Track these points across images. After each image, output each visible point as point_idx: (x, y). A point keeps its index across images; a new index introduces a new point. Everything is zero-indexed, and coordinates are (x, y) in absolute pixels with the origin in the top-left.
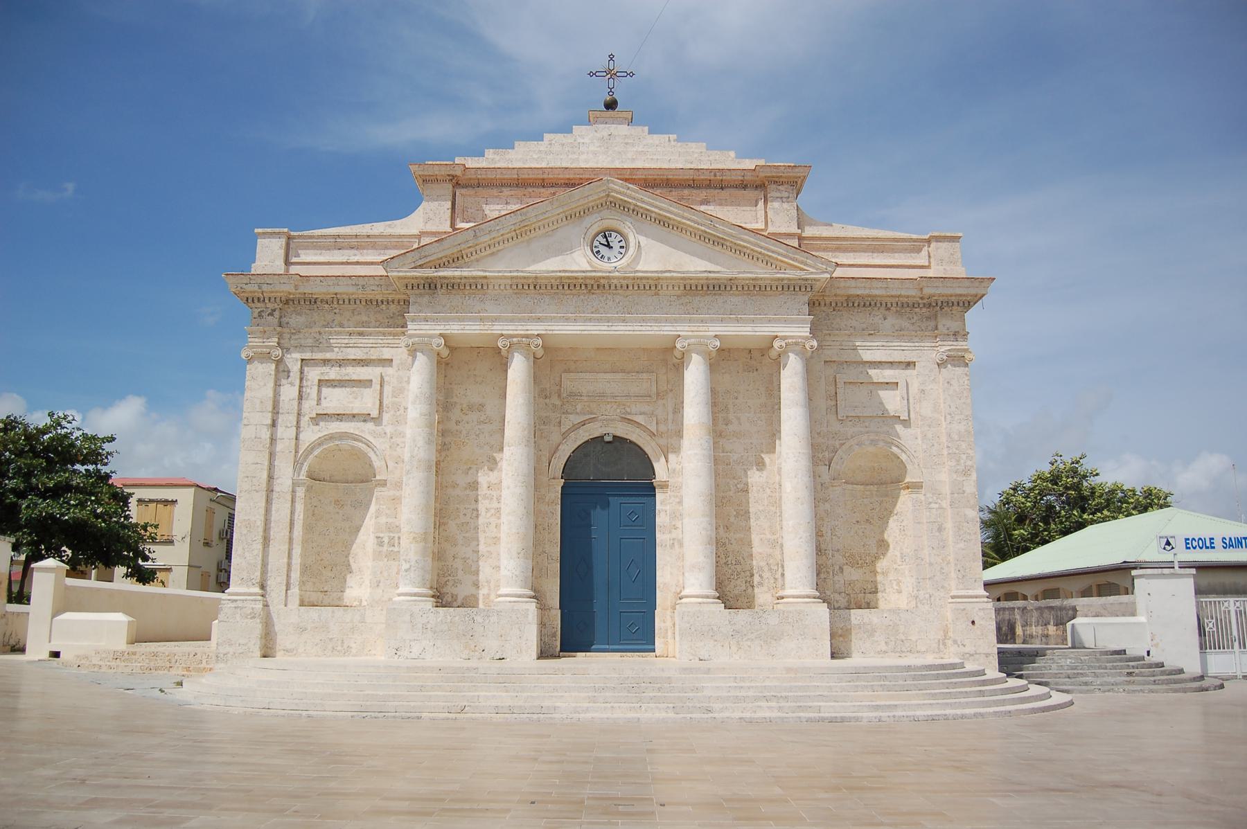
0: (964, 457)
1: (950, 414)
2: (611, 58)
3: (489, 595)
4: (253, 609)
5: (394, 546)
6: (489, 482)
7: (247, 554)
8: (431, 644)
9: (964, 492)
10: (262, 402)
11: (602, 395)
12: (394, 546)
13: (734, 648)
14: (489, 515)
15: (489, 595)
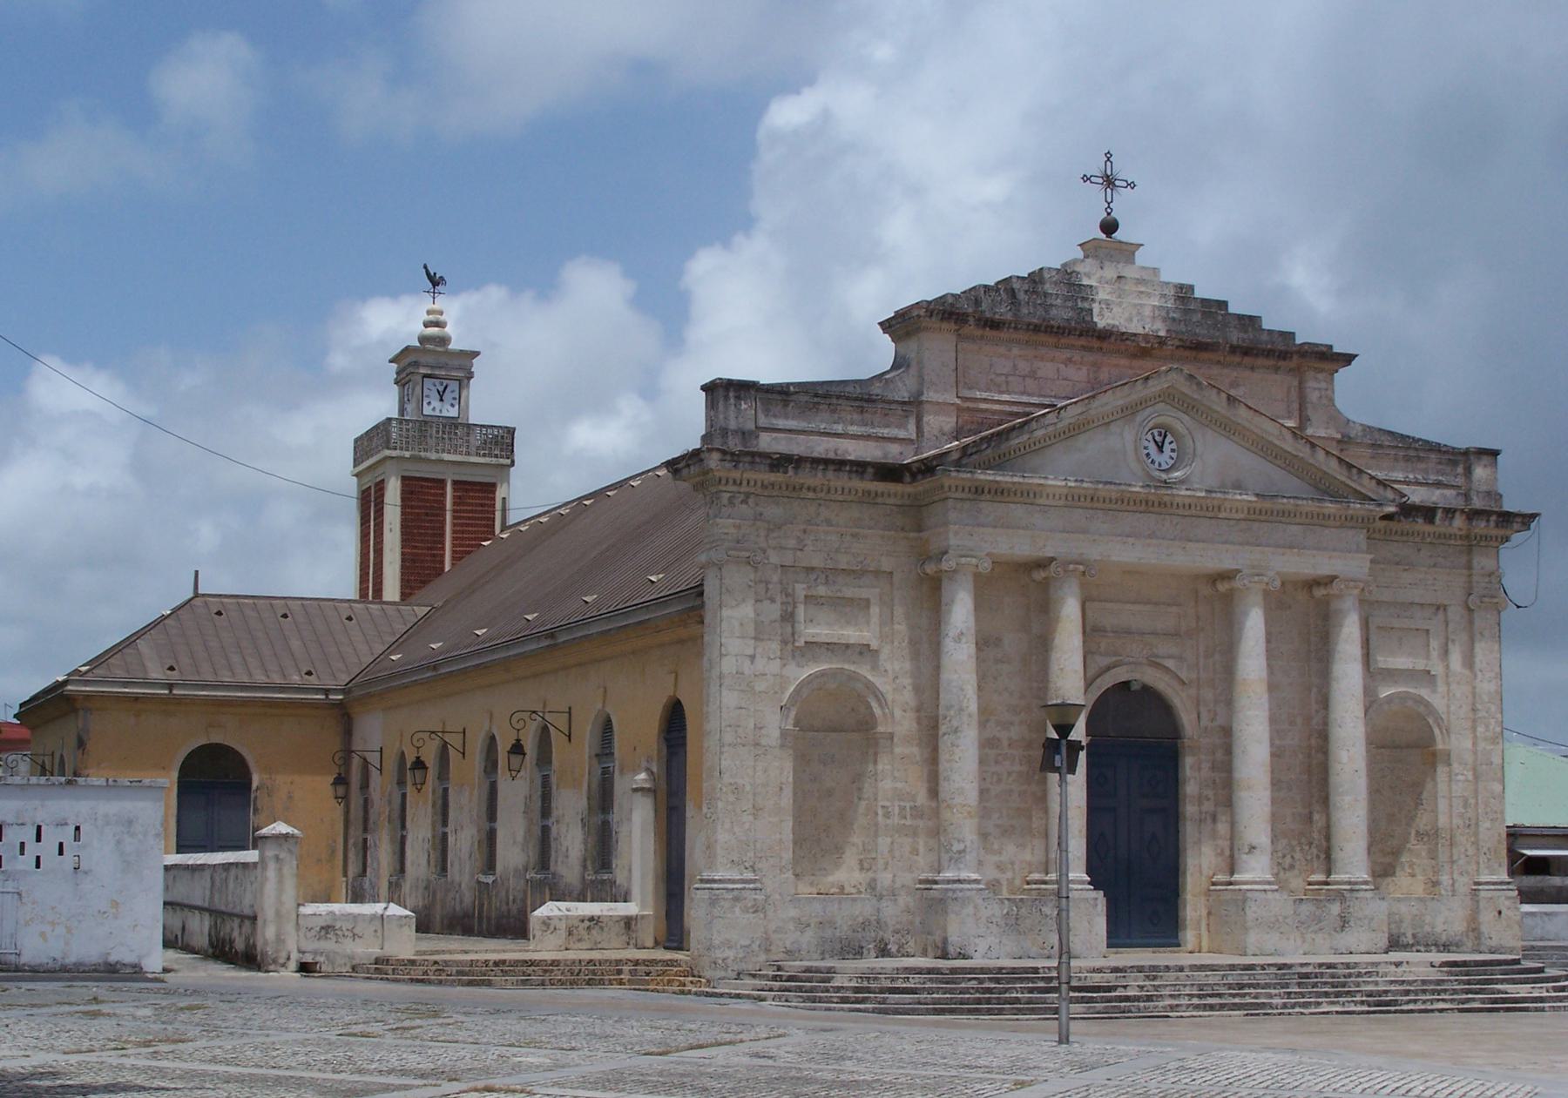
0: (1493, 721)
1: (1481, 671)
2: (1088, 179)
3: (1013, 879)
4: (755, 900)
5: (905, 818)
6: (1010, 739)
7: (736, 829)
8: (997, 941)
9: (1492, 763)
10: (741, 624)
11: (1128, 632)
12: (905, 818)
13: (1299, 941)
14: (1011, 779)
15: (1013, 879)
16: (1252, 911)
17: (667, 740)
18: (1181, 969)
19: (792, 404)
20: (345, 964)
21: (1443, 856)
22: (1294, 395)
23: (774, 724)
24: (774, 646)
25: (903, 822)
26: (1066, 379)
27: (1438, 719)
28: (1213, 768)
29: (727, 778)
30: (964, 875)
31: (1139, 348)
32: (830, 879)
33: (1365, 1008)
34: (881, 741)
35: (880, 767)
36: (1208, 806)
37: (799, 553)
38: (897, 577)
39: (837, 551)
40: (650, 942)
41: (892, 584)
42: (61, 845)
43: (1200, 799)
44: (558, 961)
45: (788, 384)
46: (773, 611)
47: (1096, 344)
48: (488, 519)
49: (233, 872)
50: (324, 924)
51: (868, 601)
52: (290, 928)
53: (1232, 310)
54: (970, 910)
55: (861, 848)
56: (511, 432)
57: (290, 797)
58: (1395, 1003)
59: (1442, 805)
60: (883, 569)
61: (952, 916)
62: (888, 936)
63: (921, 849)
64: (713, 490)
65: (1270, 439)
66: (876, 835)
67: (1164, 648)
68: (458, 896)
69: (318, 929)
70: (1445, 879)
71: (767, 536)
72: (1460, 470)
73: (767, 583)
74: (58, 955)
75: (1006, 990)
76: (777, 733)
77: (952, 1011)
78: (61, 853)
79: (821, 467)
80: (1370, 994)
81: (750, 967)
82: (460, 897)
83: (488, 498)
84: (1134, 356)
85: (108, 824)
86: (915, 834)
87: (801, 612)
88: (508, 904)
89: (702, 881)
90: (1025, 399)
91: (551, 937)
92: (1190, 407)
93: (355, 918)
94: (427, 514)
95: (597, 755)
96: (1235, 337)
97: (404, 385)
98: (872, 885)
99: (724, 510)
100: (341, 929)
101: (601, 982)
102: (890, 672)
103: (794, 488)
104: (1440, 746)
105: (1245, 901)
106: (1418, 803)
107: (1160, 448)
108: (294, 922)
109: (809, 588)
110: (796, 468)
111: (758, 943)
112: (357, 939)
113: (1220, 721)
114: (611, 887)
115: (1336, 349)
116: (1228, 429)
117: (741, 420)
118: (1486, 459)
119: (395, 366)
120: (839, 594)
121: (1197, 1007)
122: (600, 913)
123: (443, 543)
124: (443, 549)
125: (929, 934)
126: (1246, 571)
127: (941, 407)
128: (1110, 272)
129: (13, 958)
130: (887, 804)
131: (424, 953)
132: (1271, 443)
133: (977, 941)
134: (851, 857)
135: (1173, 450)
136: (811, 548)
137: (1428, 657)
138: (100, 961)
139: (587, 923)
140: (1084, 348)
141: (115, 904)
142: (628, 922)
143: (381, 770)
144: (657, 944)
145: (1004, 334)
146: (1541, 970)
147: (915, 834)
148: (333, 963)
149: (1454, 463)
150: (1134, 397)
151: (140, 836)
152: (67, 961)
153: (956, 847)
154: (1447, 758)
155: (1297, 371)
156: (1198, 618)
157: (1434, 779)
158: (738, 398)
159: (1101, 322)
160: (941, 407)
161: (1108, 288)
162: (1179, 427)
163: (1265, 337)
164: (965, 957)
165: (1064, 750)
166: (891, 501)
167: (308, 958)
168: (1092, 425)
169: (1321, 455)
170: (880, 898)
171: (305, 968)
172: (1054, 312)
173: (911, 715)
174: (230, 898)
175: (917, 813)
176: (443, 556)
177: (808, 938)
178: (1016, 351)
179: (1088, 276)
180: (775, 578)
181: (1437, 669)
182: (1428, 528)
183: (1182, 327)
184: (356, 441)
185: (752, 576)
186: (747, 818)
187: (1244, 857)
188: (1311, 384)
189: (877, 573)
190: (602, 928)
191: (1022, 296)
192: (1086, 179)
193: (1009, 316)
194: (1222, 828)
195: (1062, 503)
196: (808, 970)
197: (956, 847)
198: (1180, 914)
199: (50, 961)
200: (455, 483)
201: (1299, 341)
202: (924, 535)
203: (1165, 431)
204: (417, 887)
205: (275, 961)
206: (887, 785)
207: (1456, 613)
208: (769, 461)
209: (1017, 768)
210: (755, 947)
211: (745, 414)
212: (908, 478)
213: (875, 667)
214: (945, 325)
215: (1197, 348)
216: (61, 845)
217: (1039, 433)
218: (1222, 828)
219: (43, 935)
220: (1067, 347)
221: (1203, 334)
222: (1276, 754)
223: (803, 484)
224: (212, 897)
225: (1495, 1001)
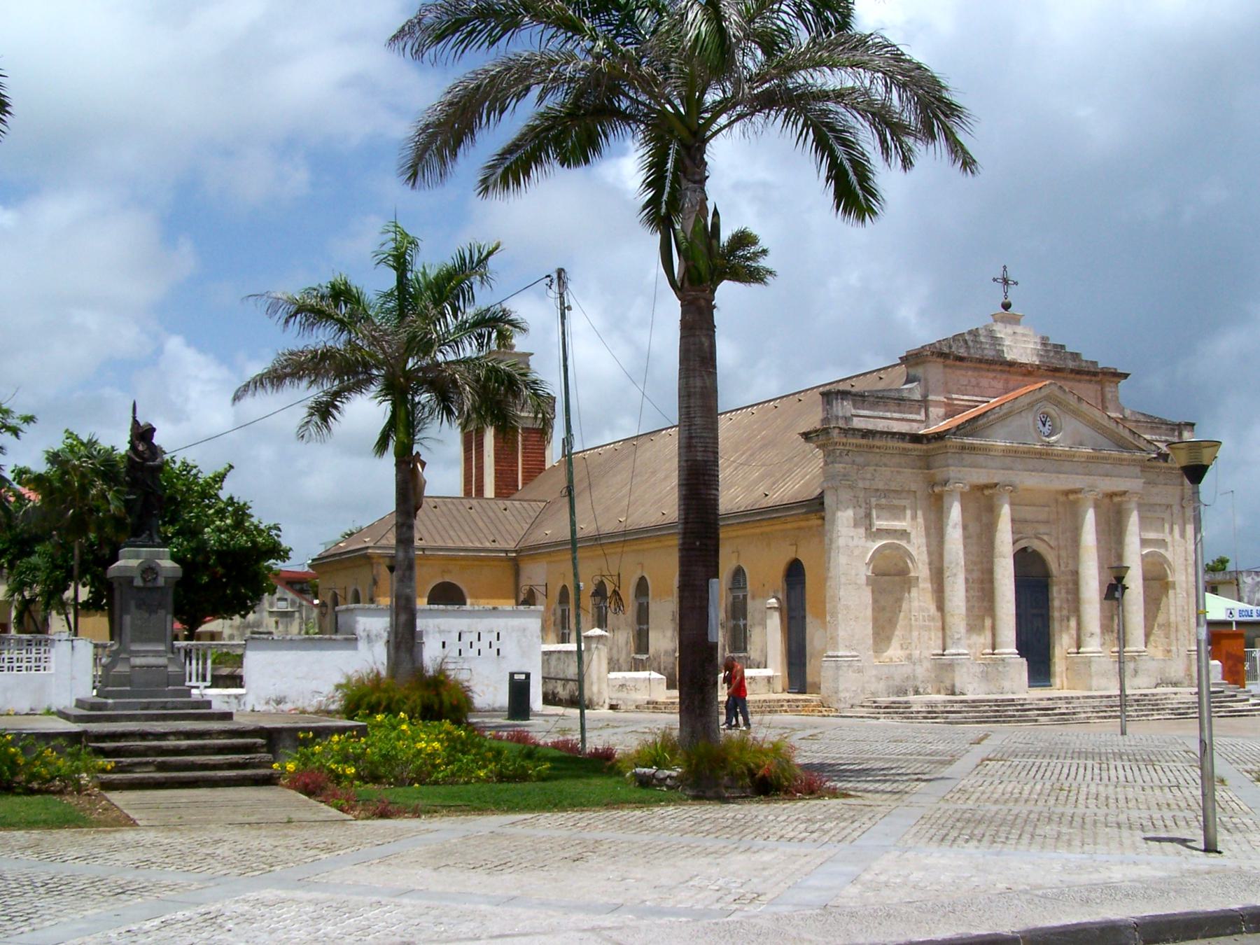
16: (1094, 668)
18: (1078, 698)
21: (1173, 636)
22: (1099, 393)
23: (864, 572)
24: (862, 531)
27: (1169, 565)
28: (1067, 592)
29: (843, 602)
30: (961, 651)
31: (1027, 371)
32: (885, 654)
33: (1173, 717)
35: (912, 595)
36: (1065, 612)
38: (918, 494)
40: (780, 690)
43: (1061, 609)
46: (862, 512)
47: (1007, 368)
49: (554, 657)
52: (604, 686)
53: (1067, 350)
54: (965, 669)
58: (1187, 714)
59: (1172, 610)
61: (957, 673)
62: (919, 684)
63: (933, 637)
64: (831, 448)
66: (911, 631)
67: (1042, 529)
70: (1174, 648)
72: (1176, 433)
75: (1006, 711)
76: (864, 578)
77: (985, 722)
80: (1172, 709)
81: (857, 702)
84: (1025, 375)
86: (930, 630)
87: (874, 513)
89: (827, 657)
90: (975, 398)
92: (1058, 403)
93: (636, 680)
96: (1071, 364)
98: (909, 657)
101: (776, 711)
104: (1170, 579)
105: (1090, 662)
106: (1158, 609)
107: (1044, 425)
110: (873, 437)
113: (1071, 567)
115: (1119, 371)
116: (1076, 414)
121: (1099, 718)
127: (938, 404)
128: (1009, 330)
131: (671, 698)
134: (895, 642)
137: (1163, 532)
142: (769, 680)
143: (546, 596)
144: (784, 690)
145: (965, 364)
146: (1235, 696)
148: (626, 704)
149: (1173, 430)
150: (1035, 398)
153: (957, 636)
154: (1173, 585)
155: (1099, 382)
156: (1058, 513)
157: (1167, 597)
158: (842, 399)
159: (1009, 356)
160: (938, 404)
161: (1010, 338)
162: (1053, 413)
163: (1084, 364)
164: (963, 694)
165: (1120, 589)
166: (915, 453)
167: (614, 702)
169: (1121, 427)
170: (915, 664)
171: (612, 707)
172: (986, 352)
173: (927, 567)
175: (932, 619)
177: (881, 686)
178: (970, 373)
179: (1000, 332)
181: (1168, 539)
182: (1165, 465)
183: (1045, 359)
188: (1108, 389)
189: (909, 491)
191: (970, 344)
192: (995, 280)
193: (966, 355)
194: (988, 622)
196: (894, 703)
197: (957, 636)
198: (1052, 669)
200: (523, 429)
201: (1100, 366)
202: (932, 471)
203: (1047, 415)
205: (598, 704)
206: (915, 604)
207: (1176, 509)
209: (977, 594)
211: (844, 408)
212: (925, 441)
213: (909, 542)
214: (939, 360)
215: (1054, 371)
217: (991, 418)
218: (1073, 623)
220: (994, 371)
221: (1057, 363)
225: (1230, 712)
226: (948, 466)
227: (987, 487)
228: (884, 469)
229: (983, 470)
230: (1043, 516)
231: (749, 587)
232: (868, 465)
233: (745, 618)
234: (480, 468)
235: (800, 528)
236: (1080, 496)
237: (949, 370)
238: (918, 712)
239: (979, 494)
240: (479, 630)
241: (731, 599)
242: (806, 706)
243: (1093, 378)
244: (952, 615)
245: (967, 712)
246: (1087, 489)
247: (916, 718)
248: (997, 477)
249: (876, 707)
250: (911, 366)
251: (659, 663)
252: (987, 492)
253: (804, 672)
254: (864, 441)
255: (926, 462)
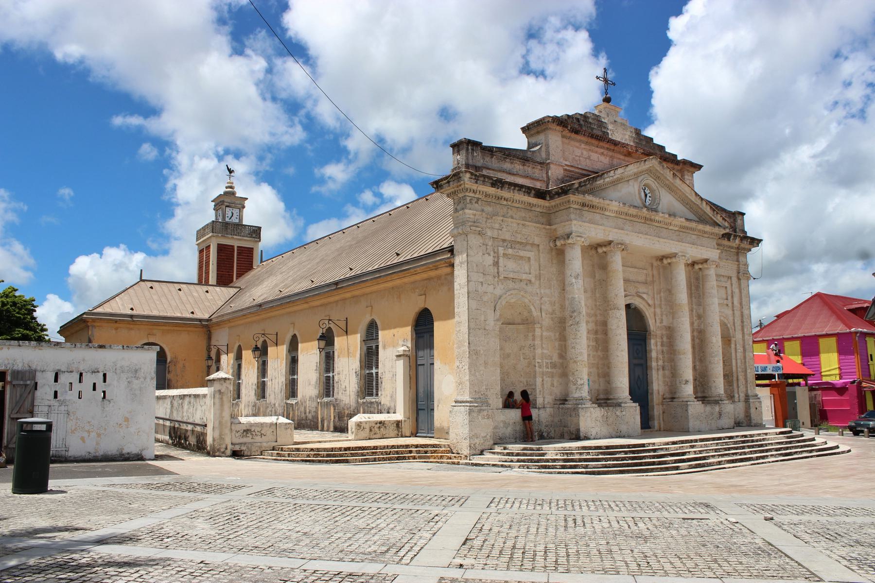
10: (477, 266)
17: (415, 330)
19: (495, 157)
20: (257, 451)
25: (547, 370)
26: (601, 162)
28: (662, 345)
34: (536, 329)
37: (500, 231)
38: (541, 247)
39: (516, 232)
41: (539, 251)
42: (94, 384)
44: (377, 447)
45: (493, 147)
47: (612, 147)
48: (250, 261)
49: (187, 399)
50: (245, 428)
51: (529, 258)
55: (525, 383)
56: (260, 228)
57: (184, 366)
60: (535, 243)
65: (687, 195)
67: (642, 289)
68: (273, 410)
69: (242, 431)
71: (486, 222)
73: (487, 245)
74: (92, 451)
78: (94, 389)
79: (512, 188)
82: (275, 410)
83: (250, 254)
85: (123, 372)
86: (552, 377)
88: (305, 413)
91: (362, 432)
93: (262, 425)
94: (227, 259)
95: (364, 341)
97: (217, 210)
99: (468, 205)
100: (254, 431)
102: (539, 295)
103: (499, 198)
108: (229, 428)
109: (505, 249)
111: (489, 434)
112: (263, 437)
114: (378, 406)
117: (474, 161)
118: (740, 216)
119: (213, 203)
120: (517, 254)
122: (384, 420)
123: (233, 270)
124: (233, 272)
125: (565, 427)
126: (680, 254)
129: (63, 453)
130: (540, 361)
132: (687, 197)
133: (592, 430)
135: (650, 197)
136: (505, 230)
138: (118, 453)
139: (378, 425)
140: (608, 149)
141: (127, 420)
142: (398, 424)
147: (552, 377)
151: (142, 379)
152: (97, 454)
153: (580, 382)
166: (538, 209)
167: (237, 448)
168: (622, 181)
172: (595, 131)
174: (185, 414)
175: (554, 366)
176: (233, 275)
178: (583, 146)
179: (604, 118)
180: (490, 243)
184: (197, 232)
185: (481, 241)
186: (482, 368)
187: (683, 386)
189: (533, 245)
190: (385, 427)
191: (582, 122)
195: (614, 215)
199: (87, 454)
202: (553, 227)
204: (249, 406)
208: (491, 181)
210: (488, 437)
216: (94, 384)
217: (607, 180)
219: (83, 439)
220: (602, 147)
222: (693, 340)
223: (502, 196)
224: (172, 412)
226: (571, 220)
227: (600, 245)
228: (510, 220)
229: (600, 227)
230: (641, 278)
231: (380, 339)
232: (497, 215)
233: (377, 367)
234: (207, 273)
235: (429, 279)
236: (674, 260)
237: (567, 141)
238: (554, 460)
239: (593, 252)
240: (81, 369)
241: (365, 348)
242: (435, 452)
243: (676, 167)
244: (575, 362)
245: (606, 460)
246: (680, 254)
247: (554, 467)
248: (613, 235)
249: (508, 454)
250: (532, 135)
251: (305, 408)
252: (600, 250)
253: (432, 417)
254: (492, 190)
255: (548, 218)
